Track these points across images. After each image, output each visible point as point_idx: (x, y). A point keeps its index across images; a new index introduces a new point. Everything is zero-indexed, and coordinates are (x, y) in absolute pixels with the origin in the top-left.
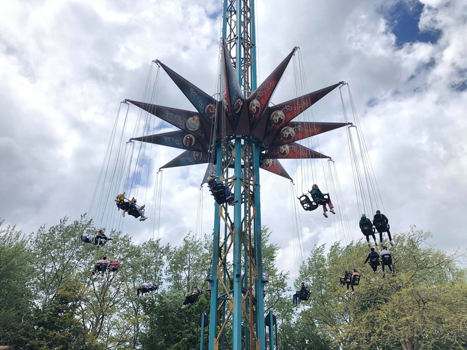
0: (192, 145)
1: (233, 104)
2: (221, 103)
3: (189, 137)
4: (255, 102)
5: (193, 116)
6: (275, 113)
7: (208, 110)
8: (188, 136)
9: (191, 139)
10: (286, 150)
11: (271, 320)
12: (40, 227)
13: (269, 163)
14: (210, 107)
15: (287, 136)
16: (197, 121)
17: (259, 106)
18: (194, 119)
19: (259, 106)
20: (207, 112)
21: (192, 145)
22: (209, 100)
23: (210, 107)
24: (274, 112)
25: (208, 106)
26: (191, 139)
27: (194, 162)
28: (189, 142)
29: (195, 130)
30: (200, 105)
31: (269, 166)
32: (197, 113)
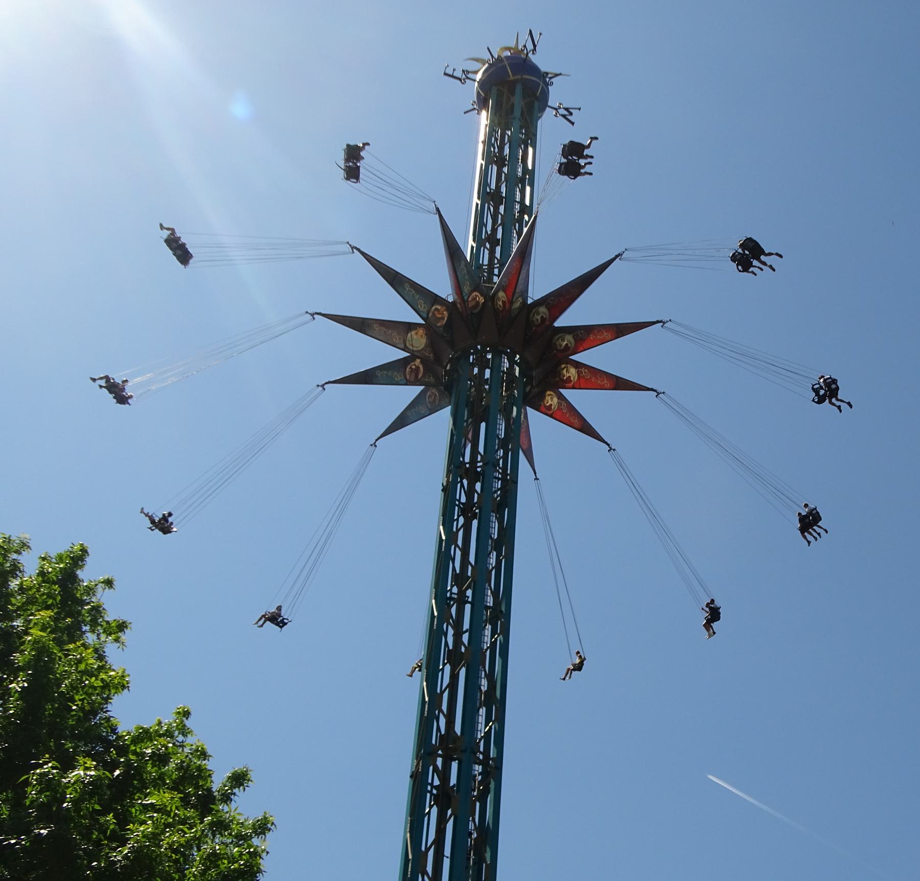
0: (420, 377)
1: (466, 298)
2: (454, 303)
3: (414, 367)
4: (501, 294)
5: (416, 329)
6: (561, 337)
7: (434, 313)
8: (413, 365)
9: (418, 368)
10: (571, 376)
11: (459, 538)
12: (156, 722)
13: (551, 405)
14: (436, 309)
15: (562, 348)
16: (422, 336)
17: (505, 299)
18: (417, 333)
19: (505, 299)
20: (432, 316)
21: (420, 377)
22: (435, 299)
23: (436, 309)
24: (534, 311)
25: (434, 308)
26: (418, 368)
27: (404, 382)
28: (413, 374)
29: (419, 349)
30: (421, 306)
31: (551, 409)
32: (423, 324)
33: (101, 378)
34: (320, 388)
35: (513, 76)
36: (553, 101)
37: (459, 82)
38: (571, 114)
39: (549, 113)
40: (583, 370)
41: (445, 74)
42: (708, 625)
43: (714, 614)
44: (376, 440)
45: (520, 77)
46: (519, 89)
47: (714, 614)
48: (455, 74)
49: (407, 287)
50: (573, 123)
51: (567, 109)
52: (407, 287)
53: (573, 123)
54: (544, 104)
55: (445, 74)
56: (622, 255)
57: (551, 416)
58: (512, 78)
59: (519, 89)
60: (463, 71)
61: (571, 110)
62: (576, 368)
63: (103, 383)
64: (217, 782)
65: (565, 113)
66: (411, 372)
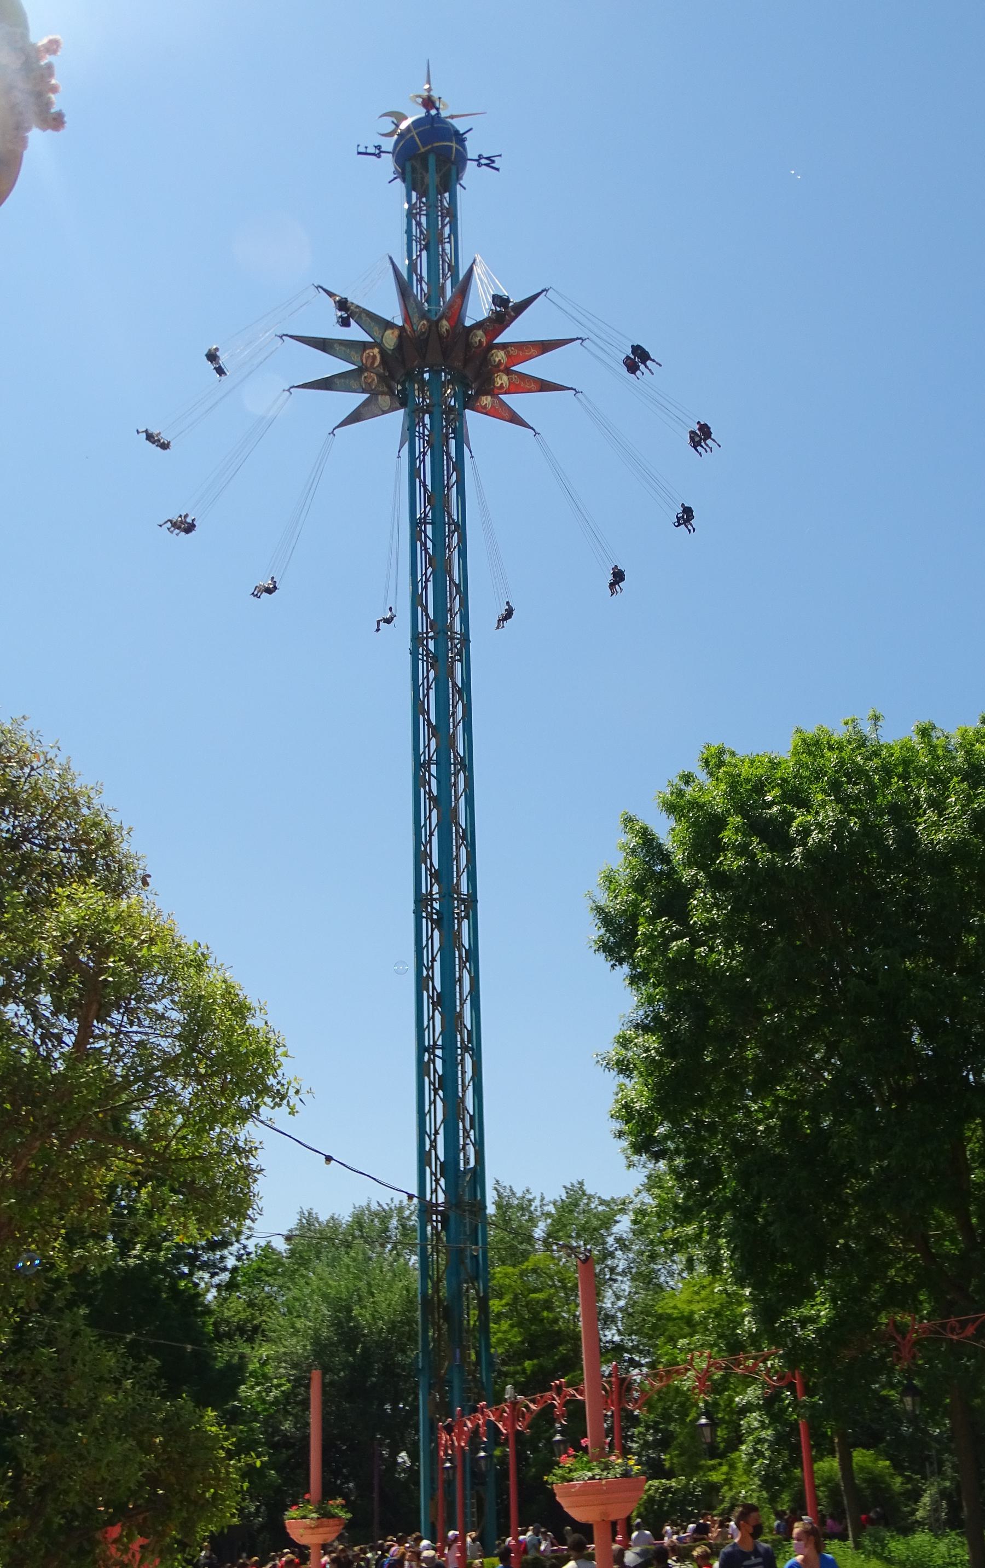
0: (375, 365)
9: (374, 357)
21: (375, 365)
33: (166, 522)
34: (288, 393)
35: (423, 147)
36: (472, 153)
37: (374, 157)
38: (493, 162)
39: (471, 166)
40: (514, 376)
41: (359, 153)
42: (612, 585)
43: (618, 576)
44: (334, 429)
45: (430, 147)
46: (432, 160)
47: (618, 576)
48: (369, 151)
49: (337, 347)
50: (497, 169)
51: (488, 158)
52: (337, 347)
53: (497, 169)
54: (461, 160)
55: (359, 153)
56: (547, 291)
57: (486, 414)
58: (423, 150)
59: (432, 160)
60: (376, 147)
61: (493, 159)
62: (507, 375)
63: (169, 525)
64: (119, 825)
65: (487, 162)
66: (367, 358)
